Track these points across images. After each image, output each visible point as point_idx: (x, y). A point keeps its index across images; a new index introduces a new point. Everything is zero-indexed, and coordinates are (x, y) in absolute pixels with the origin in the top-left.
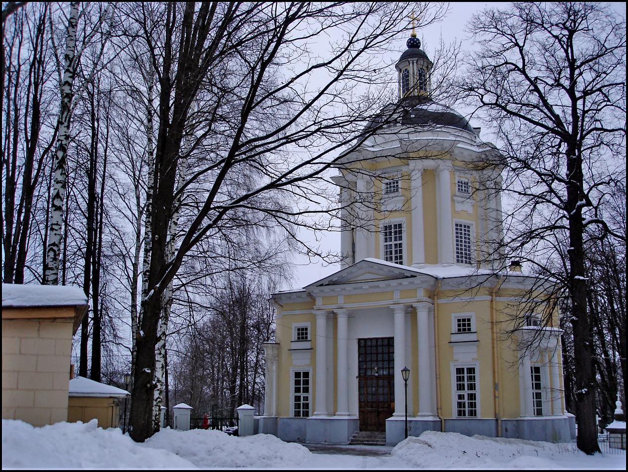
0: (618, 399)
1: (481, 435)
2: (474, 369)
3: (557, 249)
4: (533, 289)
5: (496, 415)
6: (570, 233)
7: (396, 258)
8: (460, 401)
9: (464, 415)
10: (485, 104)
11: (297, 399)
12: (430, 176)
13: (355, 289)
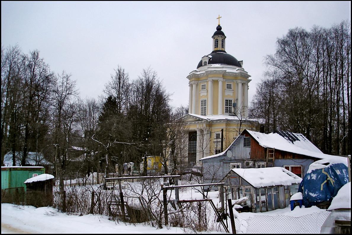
12: (215, 82)
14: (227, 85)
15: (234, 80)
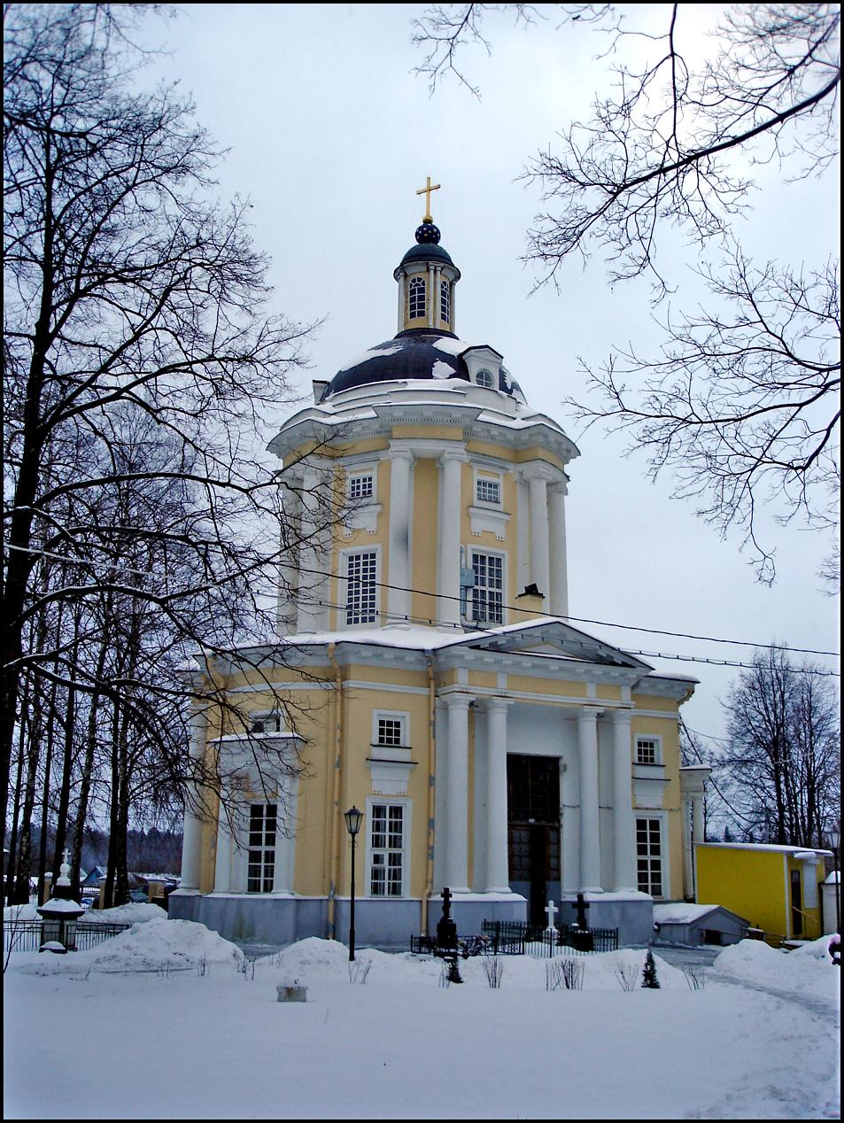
0: (66, 860)
12: (427, 468)
14: (479, 483)
15: (509, 461)
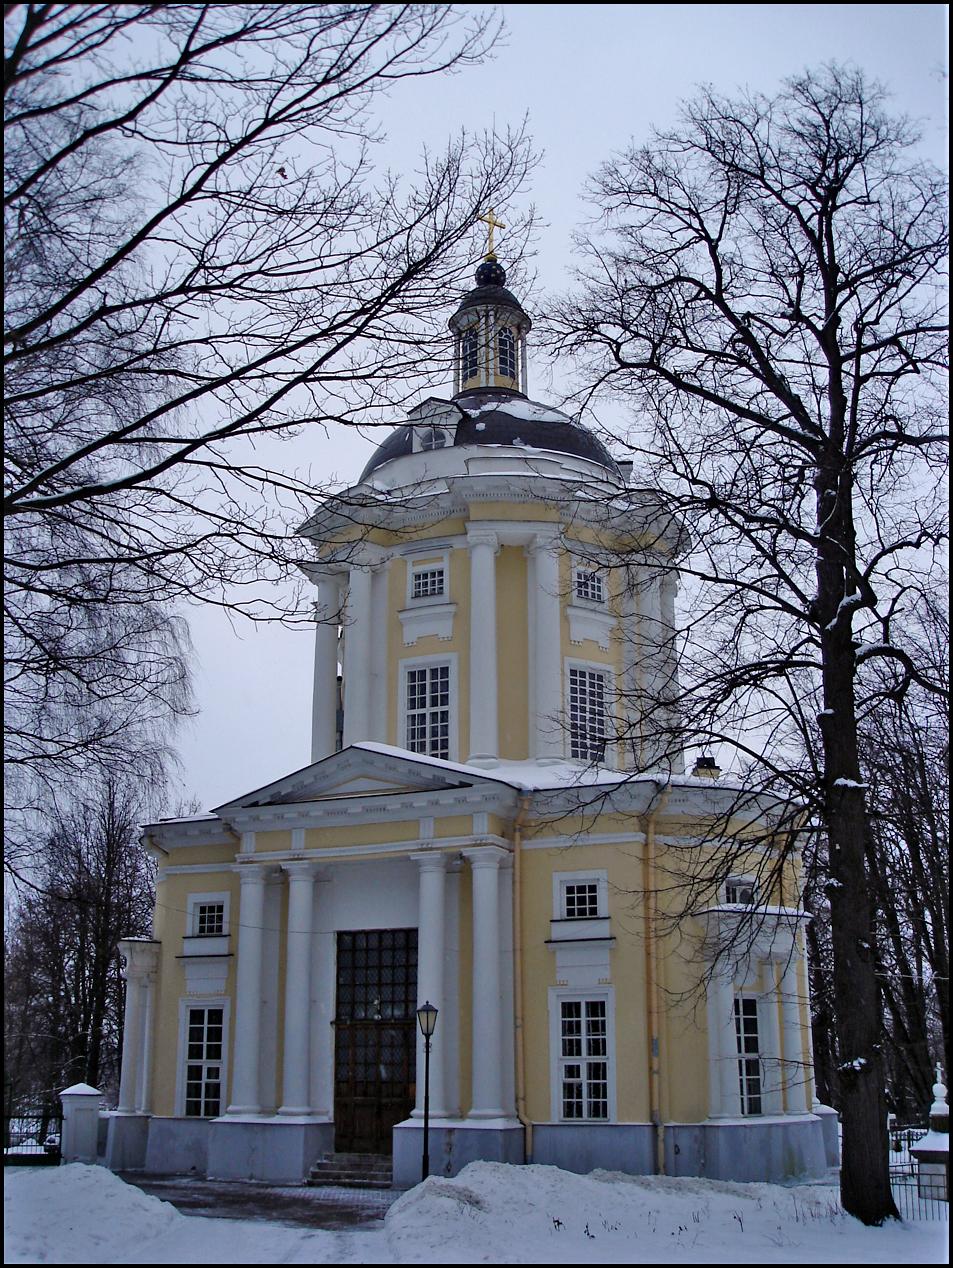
0: (939, 1078)
1: (609, 1169)
2: (603, 1004)
3: (792, 713)
4: (211, 194)
5: (652, 1115)
6: (824, 676)
7: (434, 746)
8: (571, 1080)
9: (580, 1114)
10: (624, 365)
11: (194, 1073)
12: (514, 559)
13: (329, 813)
